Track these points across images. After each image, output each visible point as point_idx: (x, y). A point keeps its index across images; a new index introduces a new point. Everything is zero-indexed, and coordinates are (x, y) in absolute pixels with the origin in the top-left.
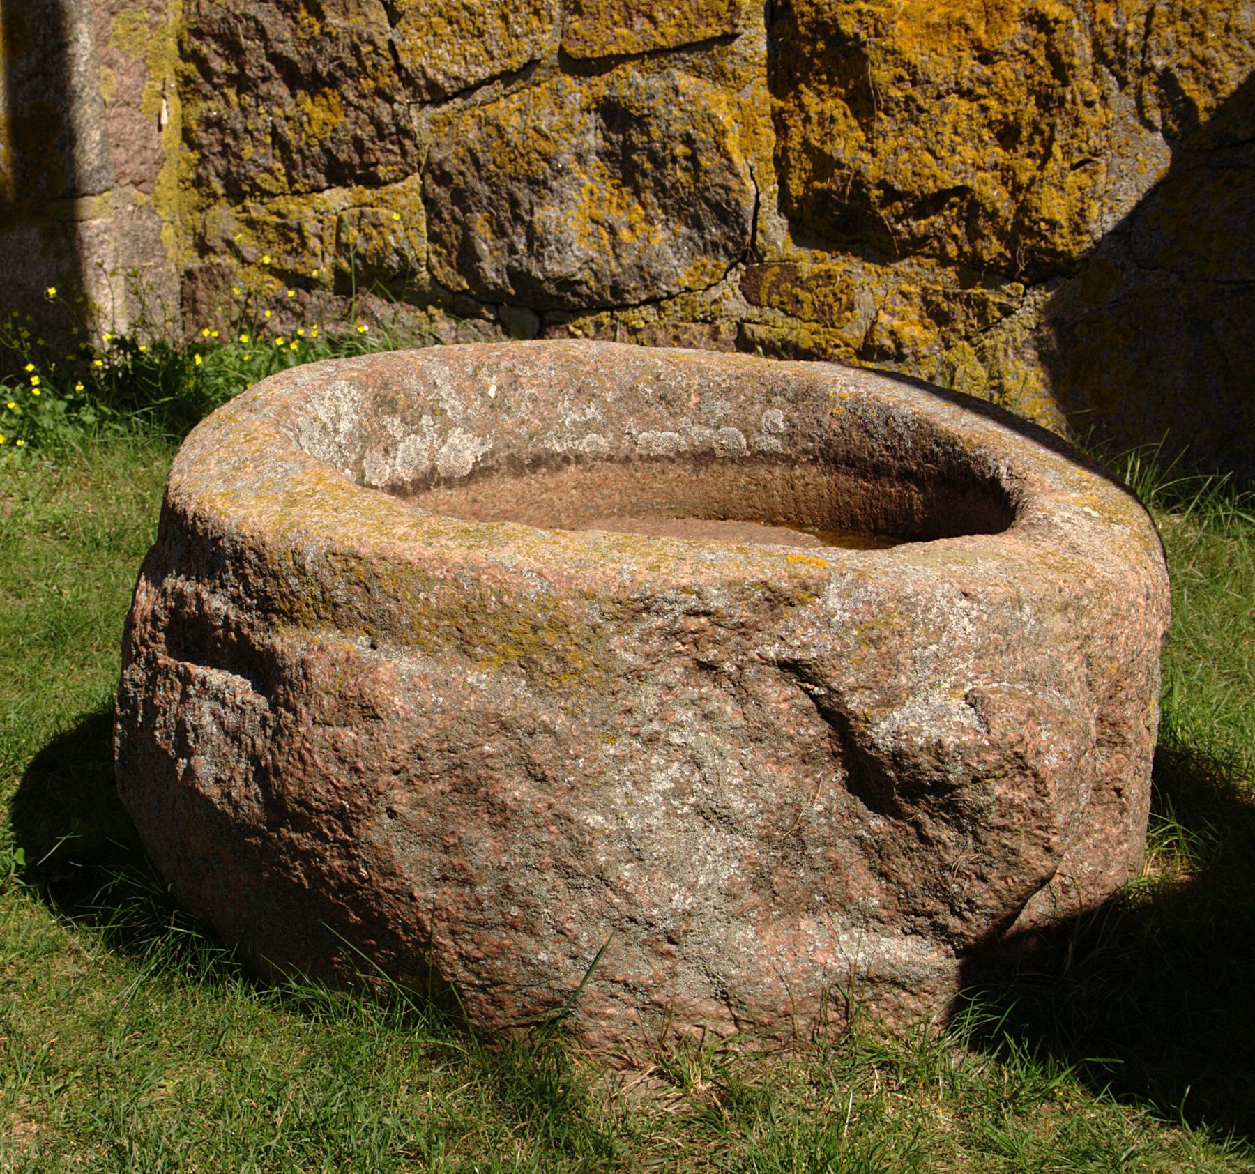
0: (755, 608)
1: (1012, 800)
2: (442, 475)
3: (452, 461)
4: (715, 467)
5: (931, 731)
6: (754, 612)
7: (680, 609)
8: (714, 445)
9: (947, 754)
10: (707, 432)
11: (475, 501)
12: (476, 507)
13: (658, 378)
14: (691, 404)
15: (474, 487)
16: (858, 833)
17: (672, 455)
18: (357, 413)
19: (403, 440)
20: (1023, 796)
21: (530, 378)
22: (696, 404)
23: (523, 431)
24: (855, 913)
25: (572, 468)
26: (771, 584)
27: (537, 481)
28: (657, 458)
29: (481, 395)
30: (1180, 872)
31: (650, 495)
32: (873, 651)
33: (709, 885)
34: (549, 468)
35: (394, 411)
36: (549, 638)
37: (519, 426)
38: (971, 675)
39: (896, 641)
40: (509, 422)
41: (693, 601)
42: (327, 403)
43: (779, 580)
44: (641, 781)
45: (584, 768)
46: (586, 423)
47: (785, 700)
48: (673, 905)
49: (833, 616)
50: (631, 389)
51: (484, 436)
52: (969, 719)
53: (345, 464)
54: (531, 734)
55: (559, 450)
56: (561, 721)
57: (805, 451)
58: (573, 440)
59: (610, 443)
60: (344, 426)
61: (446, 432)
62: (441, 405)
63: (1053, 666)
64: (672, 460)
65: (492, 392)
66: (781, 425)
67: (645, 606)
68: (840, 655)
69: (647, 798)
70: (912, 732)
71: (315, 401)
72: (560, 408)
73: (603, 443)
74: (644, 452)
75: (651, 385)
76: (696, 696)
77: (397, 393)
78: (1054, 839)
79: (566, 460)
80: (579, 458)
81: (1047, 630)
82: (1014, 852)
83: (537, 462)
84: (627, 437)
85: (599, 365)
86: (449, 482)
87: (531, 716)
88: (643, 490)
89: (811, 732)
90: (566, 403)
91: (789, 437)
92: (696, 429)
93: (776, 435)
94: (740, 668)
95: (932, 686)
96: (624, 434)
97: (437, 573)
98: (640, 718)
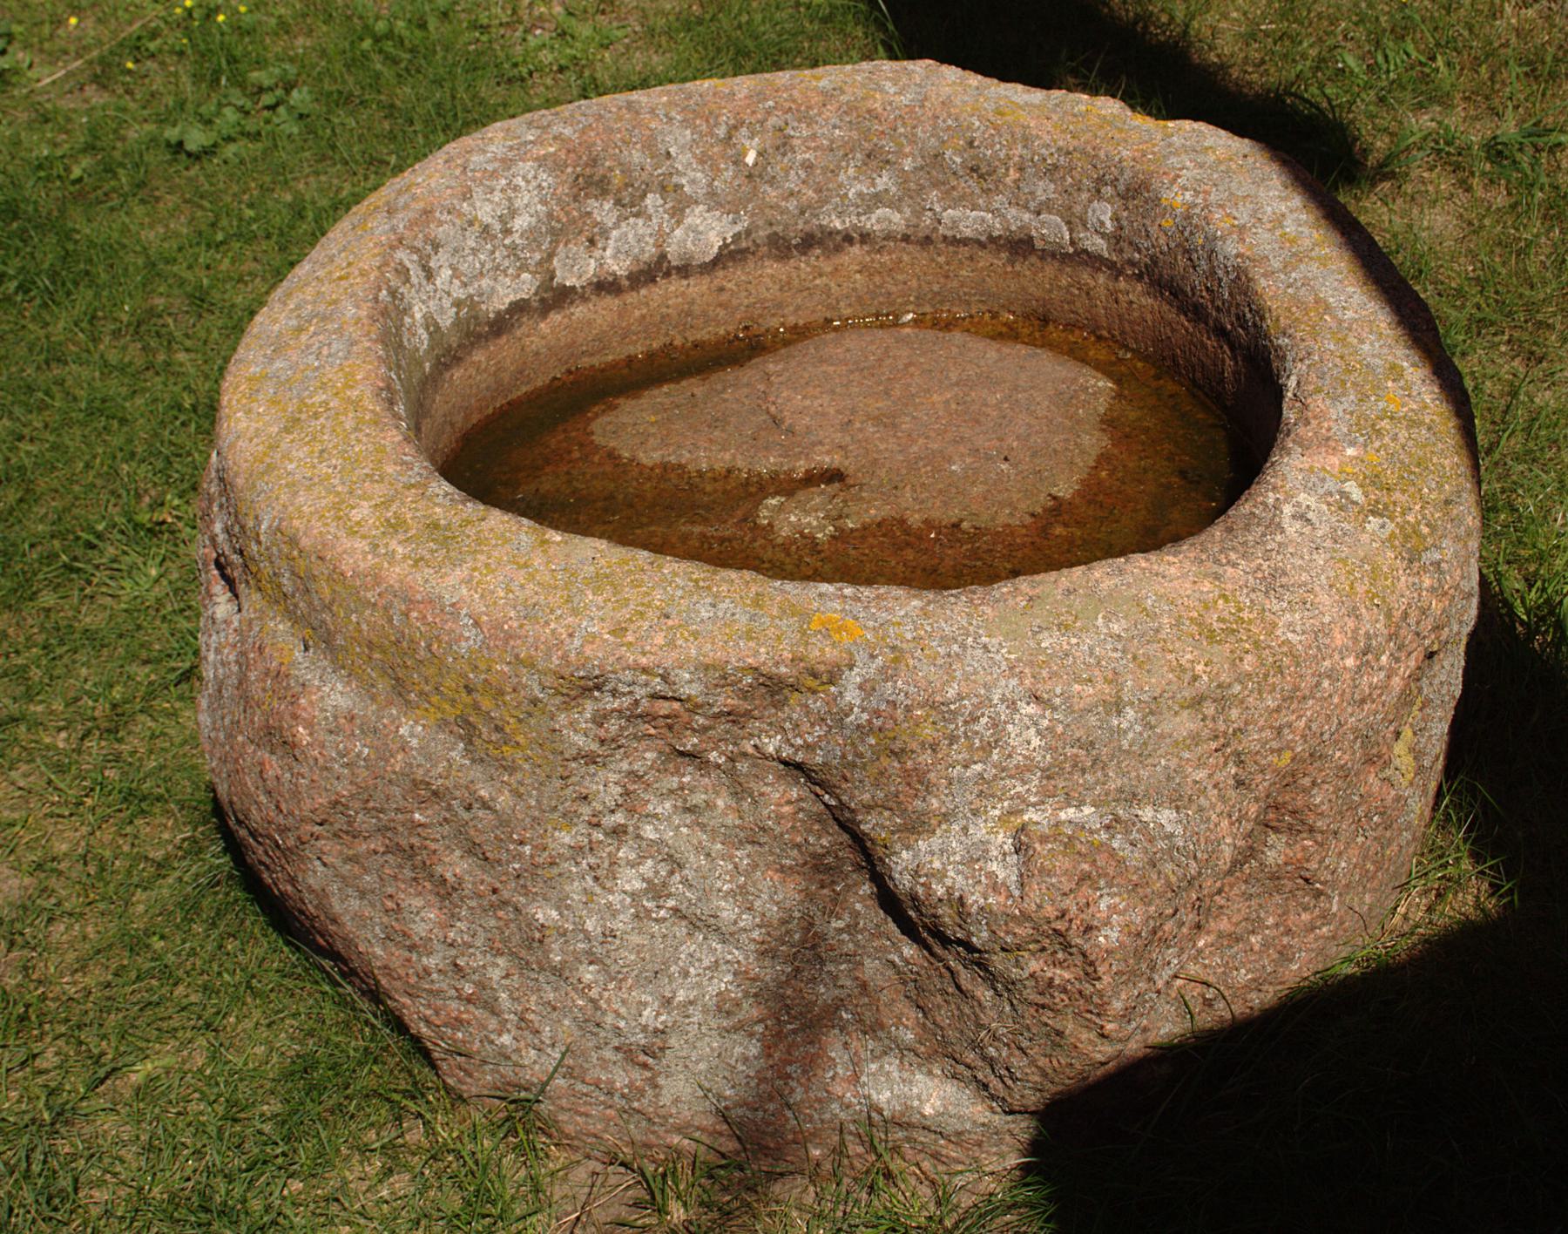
0: (744, 695)
1: (1051, 979)
2: (674, 263)
3: (689, 244)
4: (1033, 259)
5: (956, 879)
6: (745, 698)
7: (640, 692)
8: (1034, 233)
9: (969, 914)
10: (1027, 216)
11: (722, 289)
12: (724, 297)
13: (971, 144)
14: (1008, 180)
15: (721, 273)
16: (891, 957)
17: (983, 238)
18: (544, 202)
19: (617, 226)
20: (1067, 975)
21: (805, 140)
22: (1015, 181)
23: (792, 205)
24: (887, 1042)
25: (856, 250)
26: (764, 670)
27: (808, 265)
28: (965, 242)
29: (735, 163)
30: (1472, 897)
31: (955, 284)
32: (896, 764)
33: (691, 1003)
34: (825, 249)
35: (604, 193)
36: (486, 704)
37: (786, 199)
38: (1033, 799)
39: (926, 758)
40: (772, 194)
41: (658, 685)
42: (497, 197)
43: (777, 664)
44: (604, 876)
45: (532, 856)
46: (876, 195)
47: (789, 802)
48: (643, 1021)
49: (847, 715)
50: (936, 156)
51: (737, 212)
52: (1006, 872)
53: (523, 268)
54: (469, 808)
55: (839, 227)
56: (504, 800)
57: (1132, 263)
58: (859, 214)
59: (907, 220)
60: (521, 223)
61: (682, 210)
62: (675, 179)
63: (1169, 778)
64: (982, 245)
65: (750, 159)
66: (1108, 224)
67: (593, 685)
68: (853, 765)
69: (611, 898)
70: (933, 875)
71: (478, 193)
72: (842, 177)
73: (897, 220)
74: (949, 234)
75: (959, 152)
76: (675, 786)
77: (611, 169)
78: (1110, 1027)
79: (848, 239)
80: (865, 237)
81: (1162, 736)
82: (1060, 1033)
83: (809, 242)
84: (929, 213)
85: (899, 123)
86: (684, 271)
87: (467, 788)
88: (947, 277)
89: (824, 842)
90: (851, 171)
91: (1116, 239)
92: (1013, 211)
93: (1103, 235)
94: (732, 760)
95: (975, 813)
96: (924, 209)
97: (369, 595)
98: (599, 807)
